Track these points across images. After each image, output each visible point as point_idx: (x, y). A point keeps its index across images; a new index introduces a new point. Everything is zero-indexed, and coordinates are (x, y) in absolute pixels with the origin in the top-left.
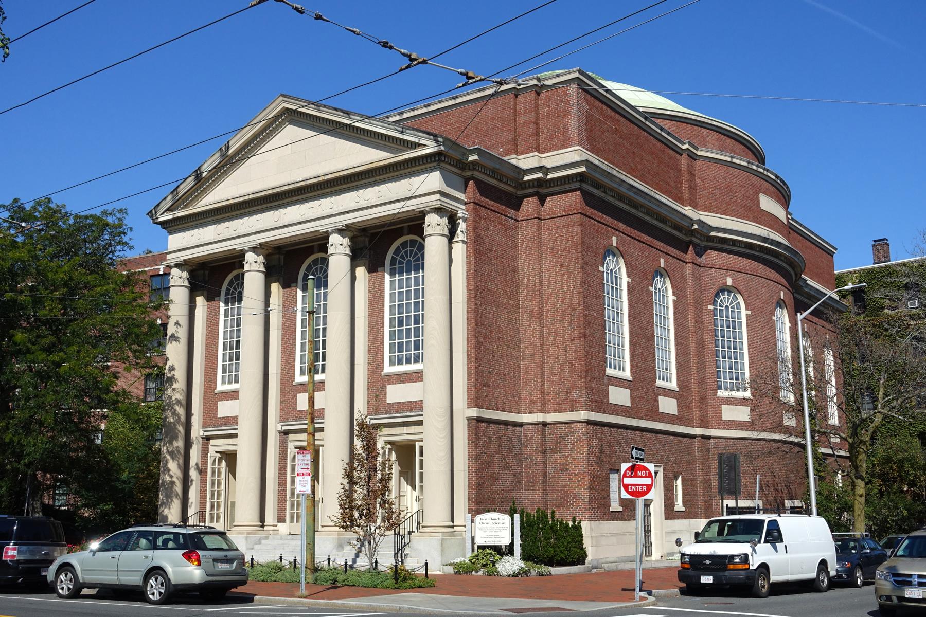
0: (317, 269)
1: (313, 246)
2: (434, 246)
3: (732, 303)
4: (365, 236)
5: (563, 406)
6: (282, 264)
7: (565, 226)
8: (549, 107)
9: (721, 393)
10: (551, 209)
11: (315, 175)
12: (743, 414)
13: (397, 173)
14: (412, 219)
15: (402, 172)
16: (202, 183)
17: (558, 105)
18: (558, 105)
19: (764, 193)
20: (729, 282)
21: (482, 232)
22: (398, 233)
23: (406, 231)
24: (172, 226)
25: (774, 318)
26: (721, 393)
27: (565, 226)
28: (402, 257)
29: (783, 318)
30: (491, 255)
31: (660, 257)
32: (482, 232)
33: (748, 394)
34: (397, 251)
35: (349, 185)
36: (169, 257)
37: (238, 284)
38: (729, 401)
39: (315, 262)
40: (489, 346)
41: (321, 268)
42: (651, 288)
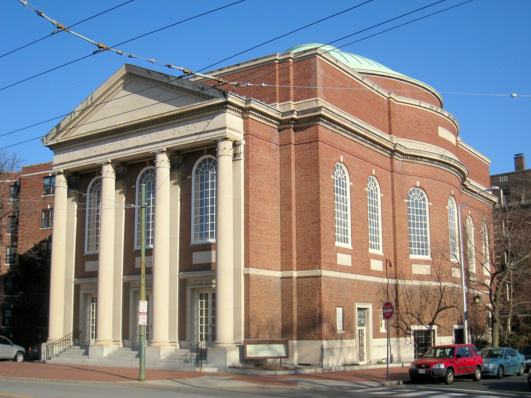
0: (148, 177)
1: (146, 162)
2: (225, 160)
3: (420, 198)
4: (179, 155)
5: (307, 266)
6: (126, 173)
7: (309, 149)
8: (299, 71)
9: (412, 256)
10: (300, 138)
11: (141, 118)
12: (425, 270)
13: (200, 115)
14: (208, 145)
15: (202, 114)
16: (73, 124)
17: (304, 70)
18: (304, 70)
19: (441, 126)
20: (418, 184)
21: (254, 153)
22: (144, 164)
23: (205, 152)
24: (57, 148)
25: (447, 207)
26: (412, 256)
27: (309, 149)
28: (203, 169)
29: (452, 205)
30: (260, 168)
31: (372, 168)
32: (254, 153)
33: (428, 257)
34: (200, 166)
35: (168, 123)
36: (54, 168)
37: (98, 186)
38: (417, 262)
39: (147, 172)
40: (258, 227)
41: (151, 176)
42: (366, 189)
